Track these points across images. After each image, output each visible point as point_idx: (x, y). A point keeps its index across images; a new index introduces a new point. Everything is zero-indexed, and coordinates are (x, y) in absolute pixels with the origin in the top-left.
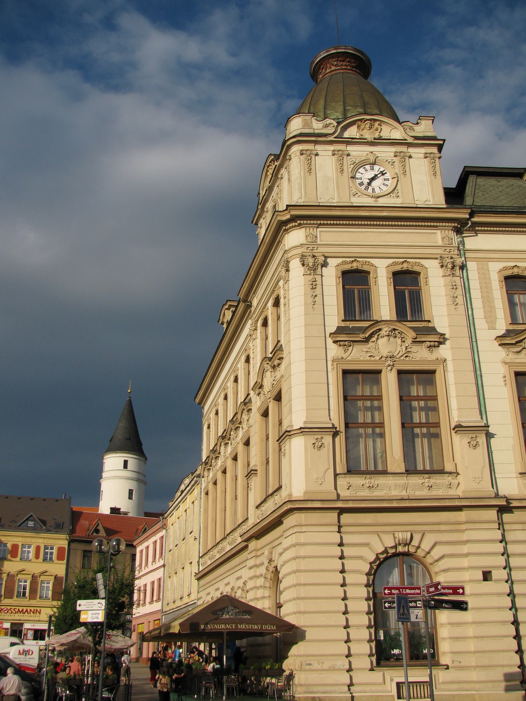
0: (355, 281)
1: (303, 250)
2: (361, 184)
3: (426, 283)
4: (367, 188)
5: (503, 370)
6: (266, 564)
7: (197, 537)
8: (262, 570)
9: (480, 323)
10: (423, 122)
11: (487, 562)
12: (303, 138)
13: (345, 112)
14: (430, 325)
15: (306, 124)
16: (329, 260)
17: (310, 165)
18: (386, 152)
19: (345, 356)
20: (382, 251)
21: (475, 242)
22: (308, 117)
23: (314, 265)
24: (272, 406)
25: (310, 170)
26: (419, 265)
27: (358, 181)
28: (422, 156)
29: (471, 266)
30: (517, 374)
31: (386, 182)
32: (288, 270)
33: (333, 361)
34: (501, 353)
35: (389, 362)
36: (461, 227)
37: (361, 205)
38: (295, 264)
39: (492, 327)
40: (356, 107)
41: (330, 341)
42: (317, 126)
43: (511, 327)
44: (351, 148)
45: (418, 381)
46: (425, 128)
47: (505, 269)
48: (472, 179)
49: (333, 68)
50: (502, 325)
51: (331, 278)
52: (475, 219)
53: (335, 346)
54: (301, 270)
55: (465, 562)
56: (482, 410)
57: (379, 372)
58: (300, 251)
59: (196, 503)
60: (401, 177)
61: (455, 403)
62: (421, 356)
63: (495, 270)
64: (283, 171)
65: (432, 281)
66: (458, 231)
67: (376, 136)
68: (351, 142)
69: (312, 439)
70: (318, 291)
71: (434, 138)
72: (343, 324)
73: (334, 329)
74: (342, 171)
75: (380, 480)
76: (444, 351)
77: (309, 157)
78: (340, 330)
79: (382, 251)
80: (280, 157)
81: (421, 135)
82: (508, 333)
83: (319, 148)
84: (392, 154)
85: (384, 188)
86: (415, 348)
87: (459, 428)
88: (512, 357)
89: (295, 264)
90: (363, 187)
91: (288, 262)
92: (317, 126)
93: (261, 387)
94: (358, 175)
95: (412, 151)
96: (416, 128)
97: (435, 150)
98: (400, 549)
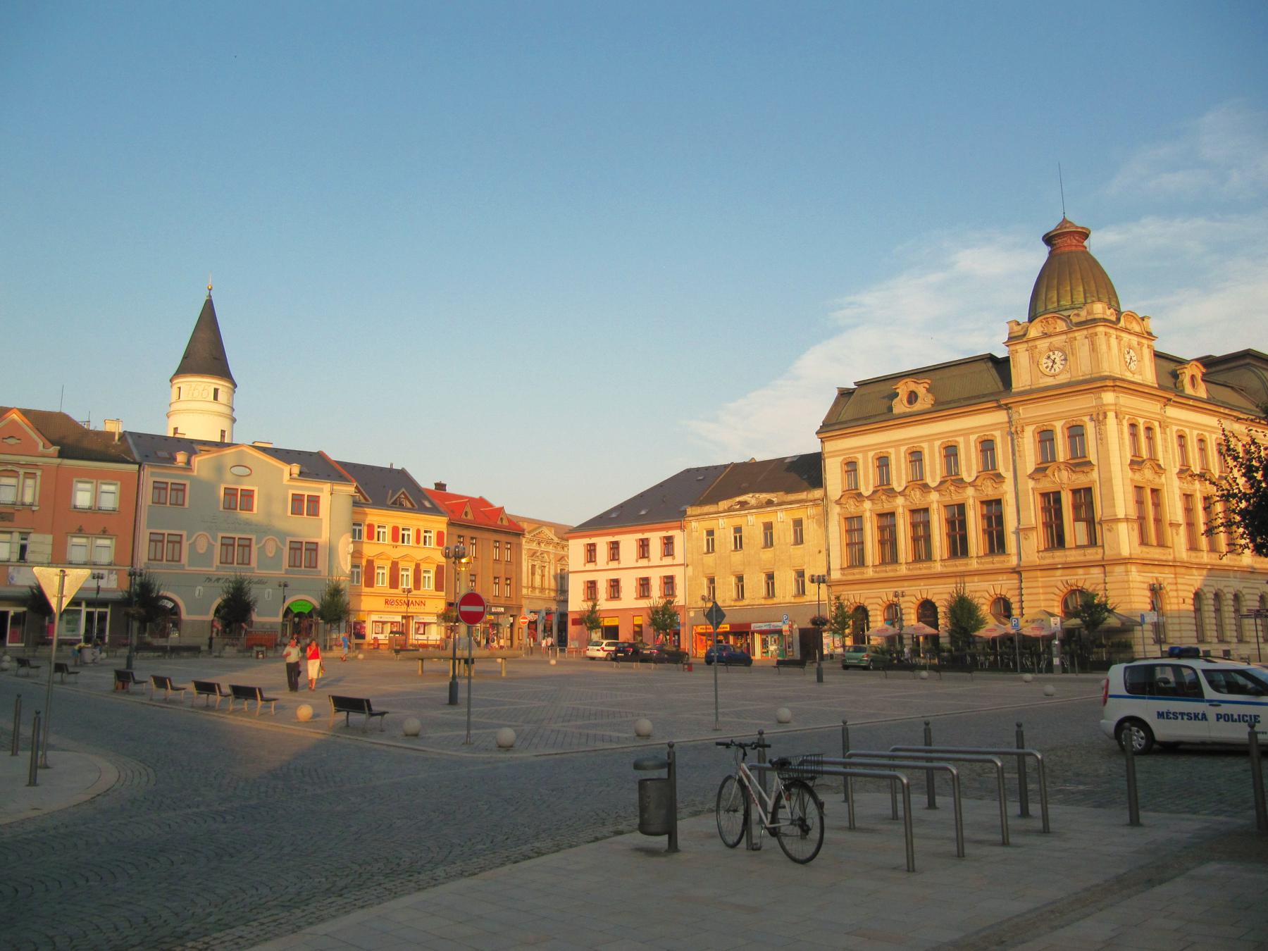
0: (1046, 437)
44: (1037, 343)
45: (1084, 498)
76: (1095, 475)
89: (1111, 415)
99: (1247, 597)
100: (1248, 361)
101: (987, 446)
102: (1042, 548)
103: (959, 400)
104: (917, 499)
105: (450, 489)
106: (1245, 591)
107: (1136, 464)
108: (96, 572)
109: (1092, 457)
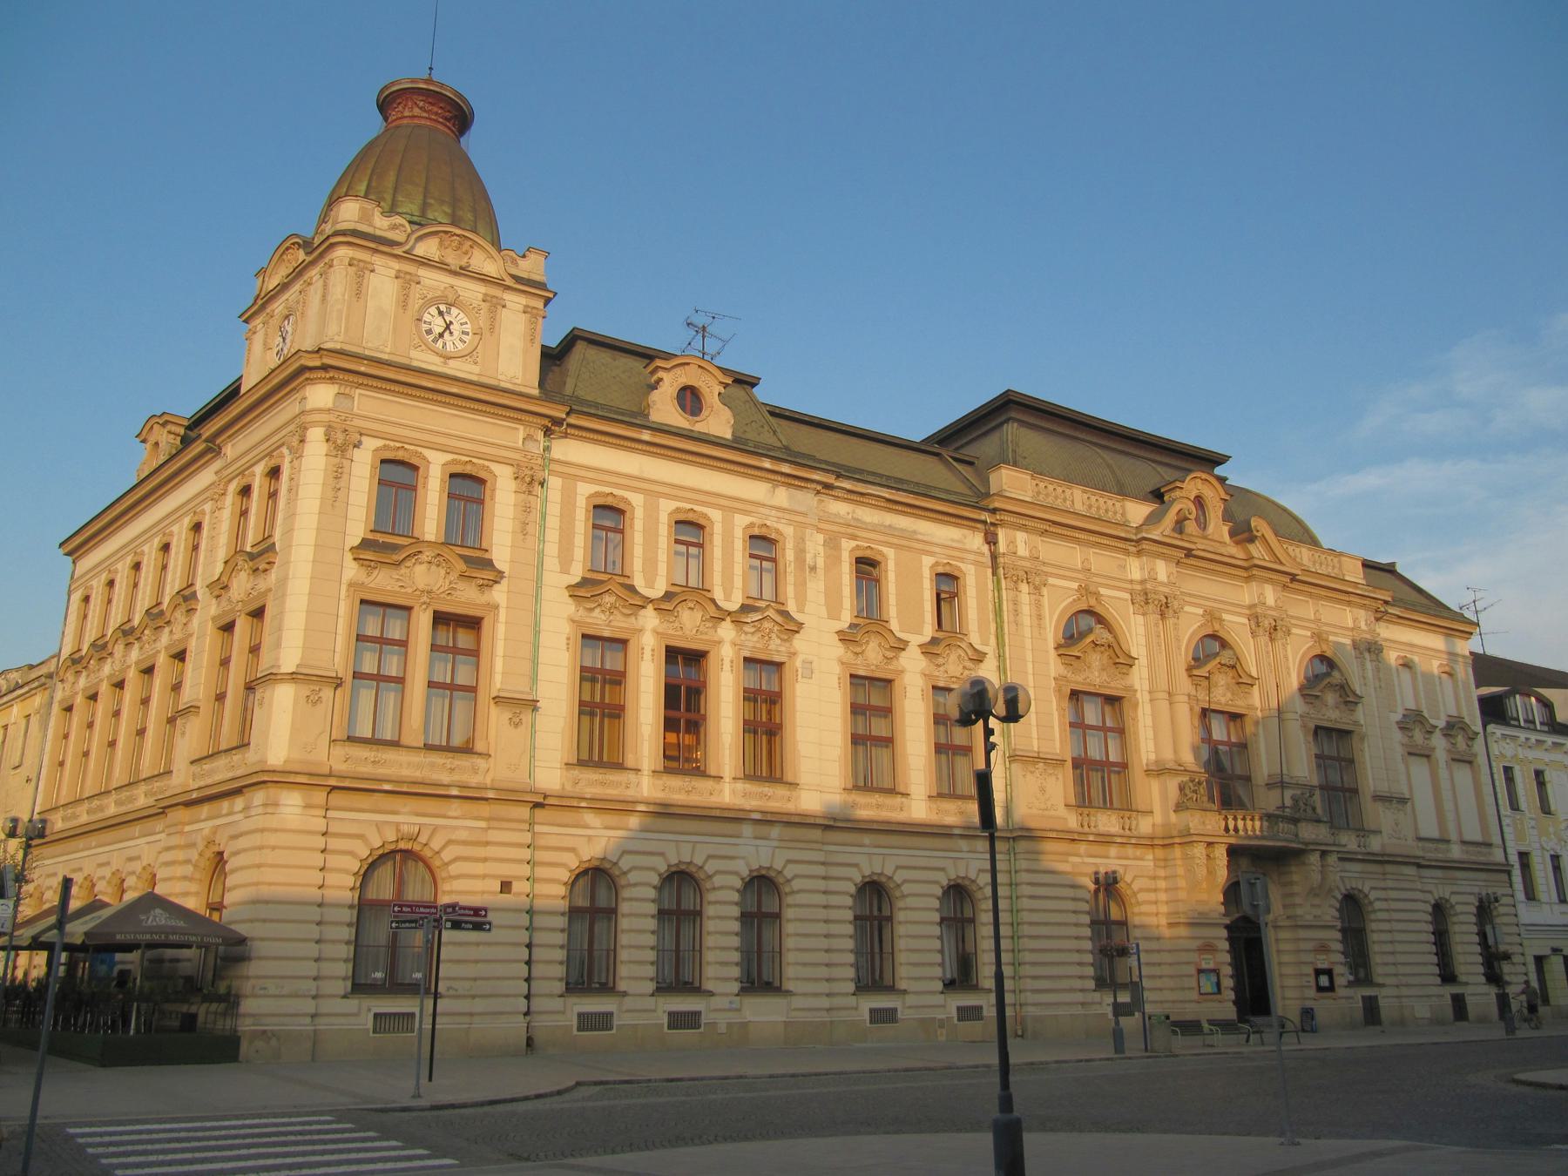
0: (398, 476)
1: (332, 417)
2: (429, 332)
3: (492, 499)
4: (435, 341)
5: (566, 628)
6: (201, 846)
7: (34, 776)
8: (194, 855)
9: (552, 563)
10: (532, 257)
11: (507, 870)
12: (356, 237)
13: (424, 208)
14: (487, 556)
15: (365, 217)
16: (364, 439)
17: (360, 284)
18: (472, 291)
19: (367, 581)
20: (442, 439)
21: (569, 450)
22: (369, 206)
23: (342, 445)
24: (242, 626)
25: (358, 294)
26: (487, 469)
27: (425, 327)
28: (521, 308)
29: (555, 483)
30: (584, 636)
31: (465, 337)
32: (302, 441)
33: (350, 585)
34: (570, 607)
35: (425, 599)
36: (553, 427)
37: (424, 366)
38: (316, 435)
39: (565, 570)
40: (442, 202)
41: (349, 556)
42: (381, 224)
43: (589, 575)
44: (423, 272)
45: (459, 627)
46: (531, 267)
47: (597, 494)
48: (580, 347)
49: (417, 111)
50: (577, 573)
51: (363, 467)
52: (572, 420)
53: (354, 565)
54: (323, 448)
55: (479, 868)
56: (534, 679)
57: (409, 609)
58: (325, 417)
59: (34, 720)
60: (486, 333)
61: (500, 667)
62: (466, 598)
63: (584, 491)
64: (314, 273)
65: (499, 495)
66: (548, 432)
67: (463, 263)
68: (425, 262)
69: (305, 690)
70: (342, 484)
71: (541, 286)
72: (370, 536)
73: (357, 542)
74: (405, 307)
75: (390, 755)
76: (499, 594)
77: (362, 271)
78: (365, 544)
79: (442, 439)
80: (316, 249)
81: (525, 275)
82: (585, 582)
83: (378, 260)
84: (480, 297)
85: (460, 346)
86: (461, 585)
87: (497, 700)
88: (582, 614)
89: (316, 435)
90: (430, 338)
91: (304, 428)
92: (381, 224)
93: (225, 587)
94: (427, 317)
95: (509, 297)
96: (521, 262)
97: (540, 304)
98: (402, 845)
99: (1459, 908)
100: (307, 375)
101: (947, 587)
102: (850, 786)
103: (888, 478)
104: (689, 627)
105: (475, 143)
106: (1454, 899)
107: (586, 590)
108: (1539, 1002)
109: (501, 555)
